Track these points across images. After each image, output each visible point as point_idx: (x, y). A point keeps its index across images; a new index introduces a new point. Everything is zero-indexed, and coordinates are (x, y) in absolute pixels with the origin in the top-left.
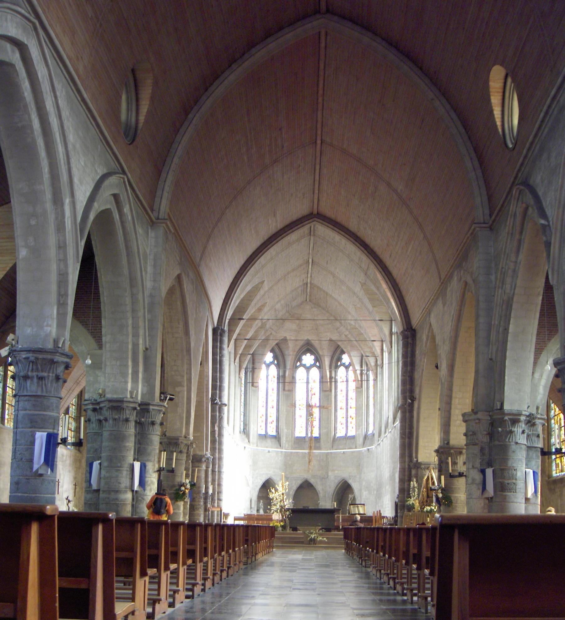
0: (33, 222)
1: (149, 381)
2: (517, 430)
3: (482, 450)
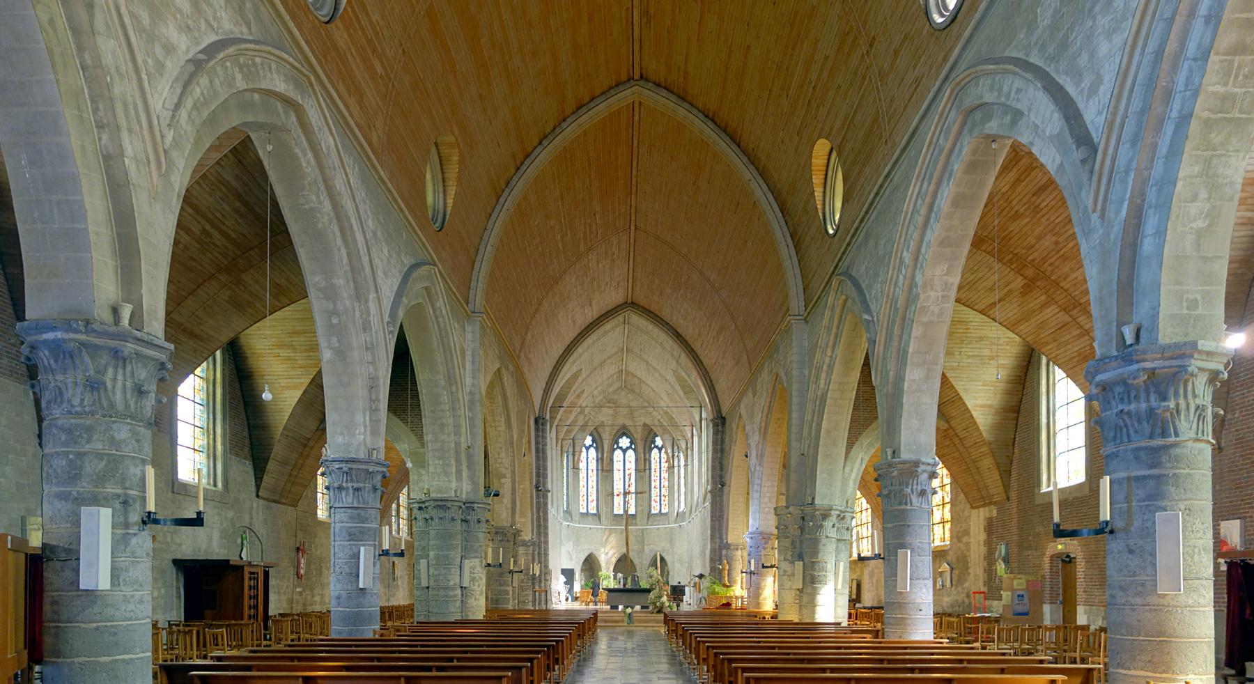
0: (335, 321)
1: (472, 478)
2: (828, 524)
3: (793, 542)
